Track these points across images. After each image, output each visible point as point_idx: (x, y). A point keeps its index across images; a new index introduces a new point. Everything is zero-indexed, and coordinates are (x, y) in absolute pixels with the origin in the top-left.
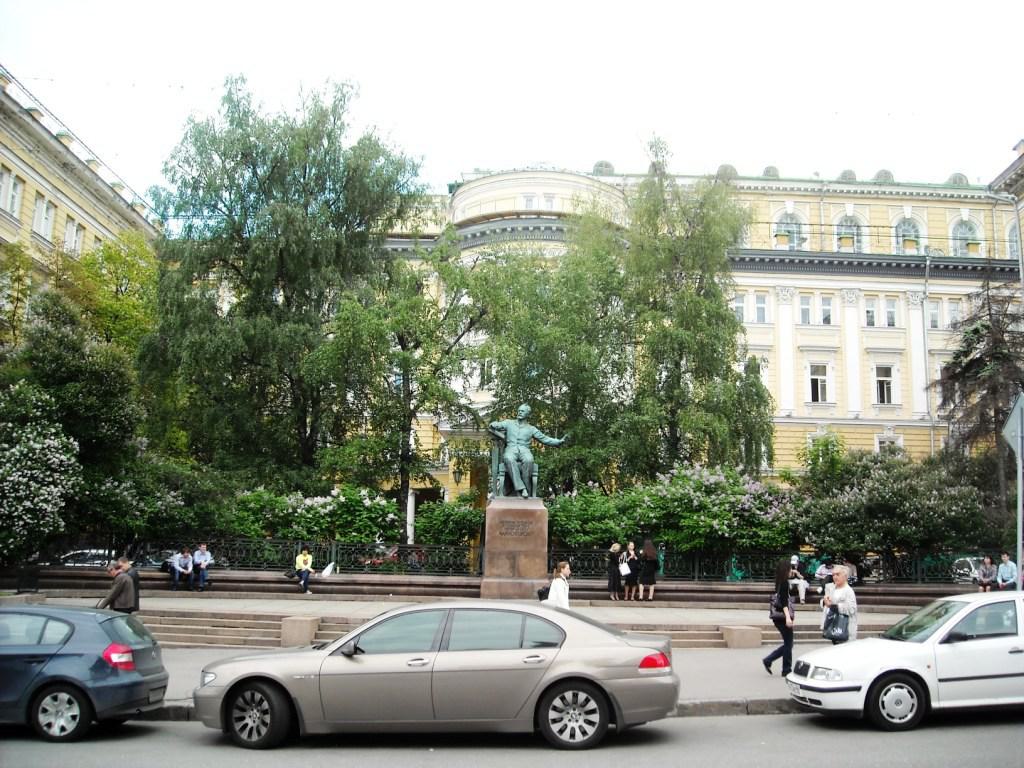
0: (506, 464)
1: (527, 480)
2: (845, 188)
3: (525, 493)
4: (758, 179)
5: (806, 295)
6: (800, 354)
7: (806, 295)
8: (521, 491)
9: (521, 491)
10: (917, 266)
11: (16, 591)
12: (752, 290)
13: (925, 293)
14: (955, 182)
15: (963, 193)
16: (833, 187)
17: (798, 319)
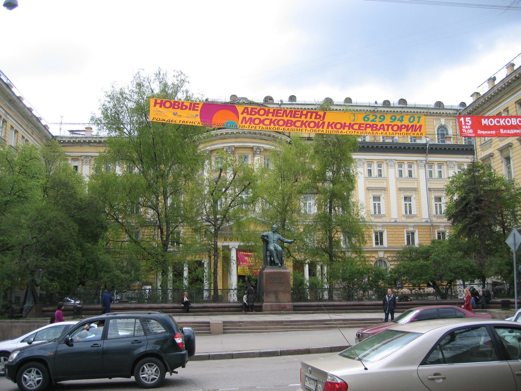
0: (270, 252)
1: (280, 259)
2: (438, 111)
3: (280, 265)
4: (433, 109)
5: (401, 164)
6: (368, 192)
7: (401, 164)
8: (278, 264)
9: (278, 264)
10: (423, 148)
11: (72, 317)
12: (437, 163)
13: (426, 161)
14: (437, 106)
15: (442, 111)
16: (432, 111)
17: (398, 175)
